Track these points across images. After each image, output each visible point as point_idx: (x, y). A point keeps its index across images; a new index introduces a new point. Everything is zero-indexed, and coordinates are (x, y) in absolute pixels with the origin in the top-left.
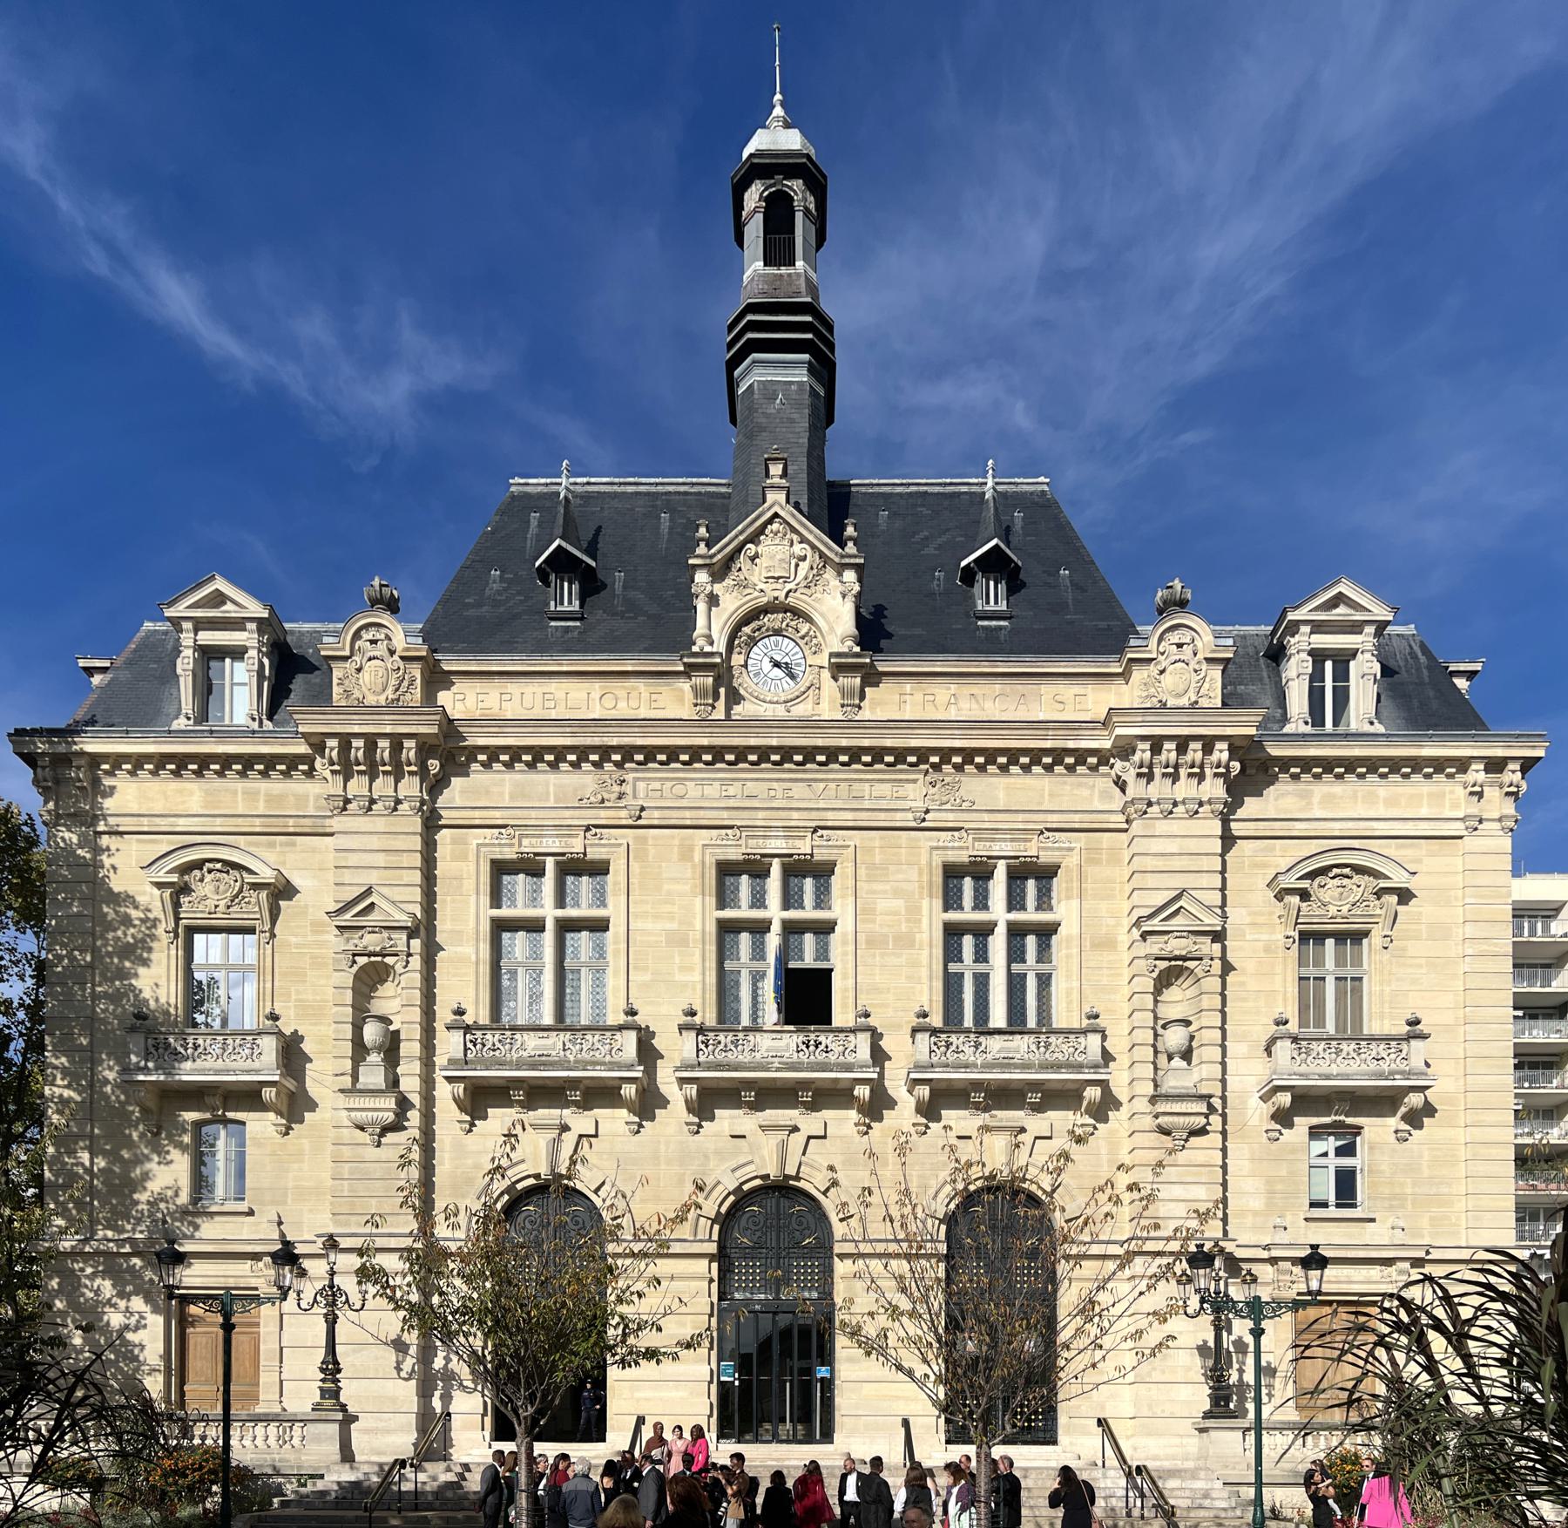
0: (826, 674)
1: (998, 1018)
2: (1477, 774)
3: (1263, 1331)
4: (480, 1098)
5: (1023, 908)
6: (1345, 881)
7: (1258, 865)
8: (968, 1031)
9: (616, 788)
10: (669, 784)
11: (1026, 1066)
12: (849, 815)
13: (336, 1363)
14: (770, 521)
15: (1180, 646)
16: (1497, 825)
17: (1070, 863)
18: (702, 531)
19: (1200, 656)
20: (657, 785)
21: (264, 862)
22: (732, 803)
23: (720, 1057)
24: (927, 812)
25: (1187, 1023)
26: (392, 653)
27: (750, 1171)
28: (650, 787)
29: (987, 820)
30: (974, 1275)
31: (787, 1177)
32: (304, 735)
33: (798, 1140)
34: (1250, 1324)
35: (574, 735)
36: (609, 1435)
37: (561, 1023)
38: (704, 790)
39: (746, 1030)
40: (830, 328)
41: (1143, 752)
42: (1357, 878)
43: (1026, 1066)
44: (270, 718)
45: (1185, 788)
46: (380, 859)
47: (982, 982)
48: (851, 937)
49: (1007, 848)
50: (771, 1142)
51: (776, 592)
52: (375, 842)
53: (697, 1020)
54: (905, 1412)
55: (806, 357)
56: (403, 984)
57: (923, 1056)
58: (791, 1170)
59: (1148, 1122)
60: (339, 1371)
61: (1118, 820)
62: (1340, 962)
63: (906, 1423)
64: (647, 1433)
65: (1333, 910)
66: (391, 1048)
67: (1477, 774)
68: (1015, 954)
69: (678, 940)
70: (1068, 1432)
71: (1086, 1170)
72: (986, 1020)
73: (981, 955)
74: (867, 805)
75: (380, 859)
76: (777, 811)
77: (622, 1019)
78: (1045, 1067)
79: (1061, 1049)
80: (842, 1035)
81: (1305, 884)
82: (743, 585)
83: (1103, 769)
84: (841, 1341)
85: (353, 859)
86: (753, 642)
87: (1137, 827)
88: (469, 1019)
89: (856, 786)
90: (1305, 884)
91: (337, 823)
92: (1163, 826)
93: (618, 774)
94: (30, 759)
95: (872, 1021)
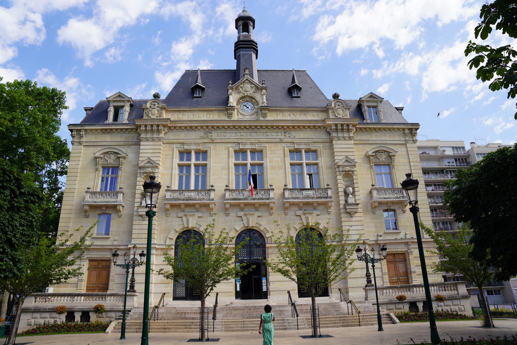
1: (192, 187)
5: (199, 160)
11: (313, 198)
18: (230, 82)
22: (237, 137)
23: (261, 197)
29: (299, 141)
34: (372, 264)
35: (200, 123)
37: (312, 188)
38: (231, 136)
40: (257, 44)
43: (313, 198)
46: (151, 151)
49: (194, 147)
52: (150, 147)
53: (90, 190)
54: (288, 289)
62: (112, 173)
63: (289, 292)
64: (104, 299)
68: (197, 171)
74: (270, 137)
75: (151, 151)
76: (249, 140)
78: (318, 198)
84: (269, 269)
94: (71, 131)
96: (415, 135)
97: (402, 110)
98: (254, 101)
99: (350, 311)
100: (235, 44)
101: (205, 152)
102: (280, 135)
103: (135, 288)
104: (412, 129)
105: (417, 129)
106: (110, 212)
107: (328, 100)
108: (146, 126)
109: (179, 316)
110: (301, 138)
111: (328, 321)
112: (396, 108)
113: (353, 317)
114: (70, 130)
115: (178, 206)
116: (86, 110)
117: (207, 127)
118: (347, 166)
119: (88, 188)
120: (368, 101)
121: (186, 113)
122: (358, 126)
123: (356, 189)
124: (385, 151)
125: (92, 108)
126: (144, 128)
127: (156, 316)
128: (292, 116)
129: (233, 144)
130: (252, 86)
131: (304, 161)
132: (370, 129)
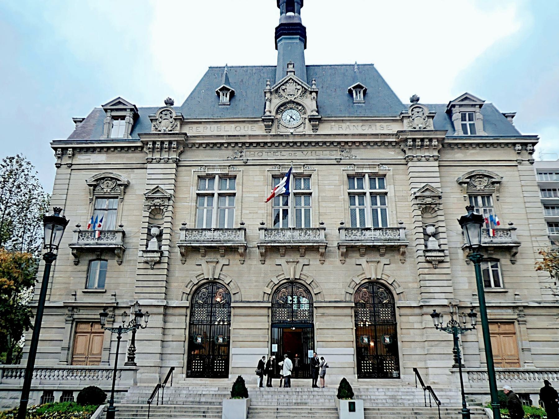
0: (307, 121)
2: (519, 147)
3: (121, 337)
4: (189, 251)
6: (481, 179)
7: (189, 178)
8: (358, 229)
9: (240, 154)
10: (256, 153)
12: (315, 161)
13: (134, 347)
14: (289, 80)
15: (418, 112)
16: (527, 162)
17: (389, 174)
19: (425, 115)
20: (253, 153)
21: (124, 177)
24: (341, 159)
25: (434, 226)
26: (171, 117)
27: (282, 277)
28: (250, 155)
30: (201, 315)
31: (215, 279)
32: (142, 141)
33: (300, 266)
36: (230, 376)
38: (268, 155)
39: (282, 229)
41: (410, 143)
42: (485, 178)
44: (131, 134)
45: (165, 156)
47: (362, 211)
48: (240, 201)
49: (369, 171)
50: (292, 267)
51: (290, 98)
53: (264, 226)
55: (299, 36)
56: (165, 215)
57: (343, 238)
58: (216, 277)
59: (423, 259)
60: (135, 350)
61: (404, 162)
65: (478, 188)
66: (159, 237)
67: (519, 147)
68: (374, 203)
69: (335, 199)
70: (231, 373)
71: (401, 275)
72: (364, 224)
73: (361, 203)
77: (239, 226)
79: (391, 235)
80: (314, 231)
81: (468, 180)
82: (281, 96)
83: (398, 146)
85: (153, 177)
86: (282, 112)
87: (410, 164)
88: (187, 227)
89: (324, 152)
90: (468, 180)
91: (149, 166)
92: (418, 164)
93: (240, 150)
94: (55, 149)
95: (124, 229)
96: (532, 152)
97: (513, 117)
98: (300, 108)
99: (428, 401)
100: (276, 29)
101: (382, 177)
102: (336, 154)
103: (136, 361)
104: (528, 144)
105: (534, 144)
106: (106, 258)
107: (404, 105)
108: (154, 143)
109: (191, 399)
110: (365, 158)
111: (293, 413)
112: (504, 114)
113: (432, 409)
114: (53, 148)
115: (196, 249)
116: (75, 122)
117: (236, 144)
118: (428, 197)
119: (183, 224)
120: (461, 106)
121: (208, 126)
122: (446, 141)
123: (146, 231)
124: (112, 178)
125: (83, 119)
126: (420, 143)
127: (160, 399)
128: (352, 128)
129: (271, 167)
130: (299, 87)
131: (216, 192)
132: (464, 144)
